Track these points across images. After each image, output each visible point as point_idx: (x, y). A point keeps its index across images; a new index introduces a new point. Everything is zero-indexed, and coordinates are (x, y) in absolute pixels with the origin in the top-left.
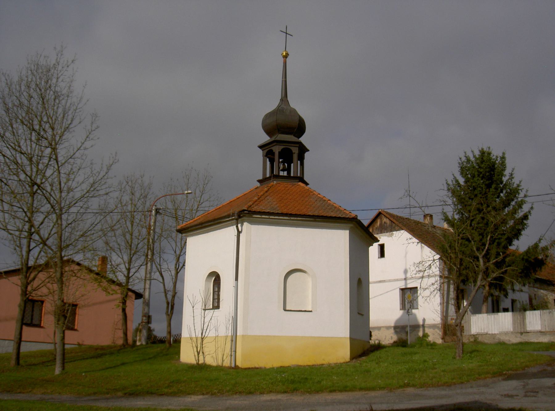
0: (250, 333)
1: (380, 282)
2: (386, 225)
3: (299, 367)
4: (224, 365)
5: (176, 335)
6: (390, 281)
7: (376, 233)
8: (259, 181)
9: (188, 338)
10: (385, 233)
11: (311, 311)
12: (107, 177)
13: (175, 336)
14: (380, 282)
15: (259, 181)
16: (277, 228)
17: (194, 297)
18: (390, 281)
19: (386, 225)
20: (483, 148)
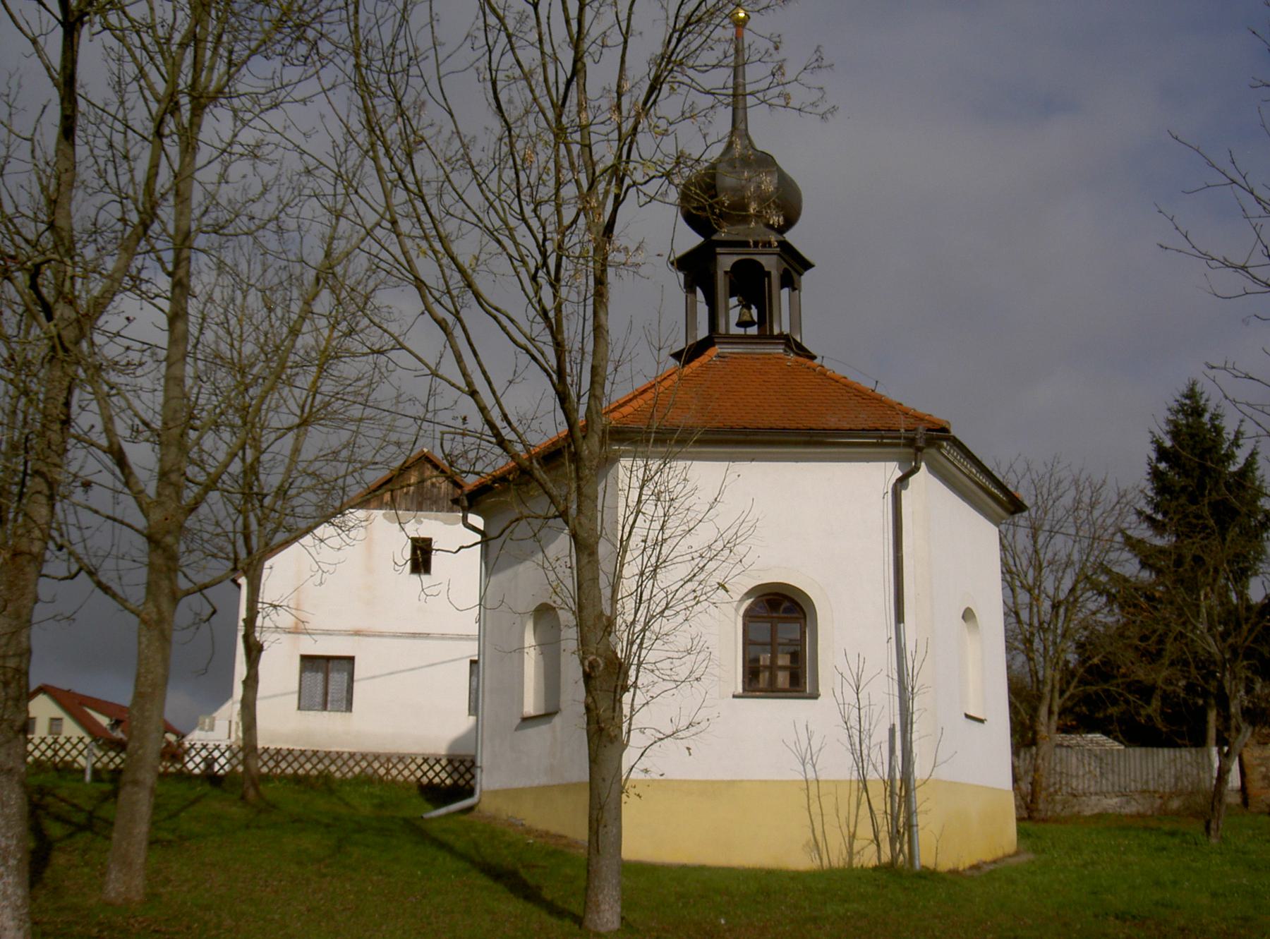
0: (943, 773)
1: (414, 635)
2: (435, 490)
3: (702, 869)
4: (856, 862)
5: (395, 761)
6: (443, 637)
7: (403, 506)
8: (677, 356)
9: (802, 781)
10: (432, 510)
11: (981, 721)
12: (421, 238)
13: (426, 760)
14: (414, 635)
15: (677, 356)
16: (960, 500)
17: (862, 660)
18: (443, 637)
19: (435, 490)
20: (1170, 406)
